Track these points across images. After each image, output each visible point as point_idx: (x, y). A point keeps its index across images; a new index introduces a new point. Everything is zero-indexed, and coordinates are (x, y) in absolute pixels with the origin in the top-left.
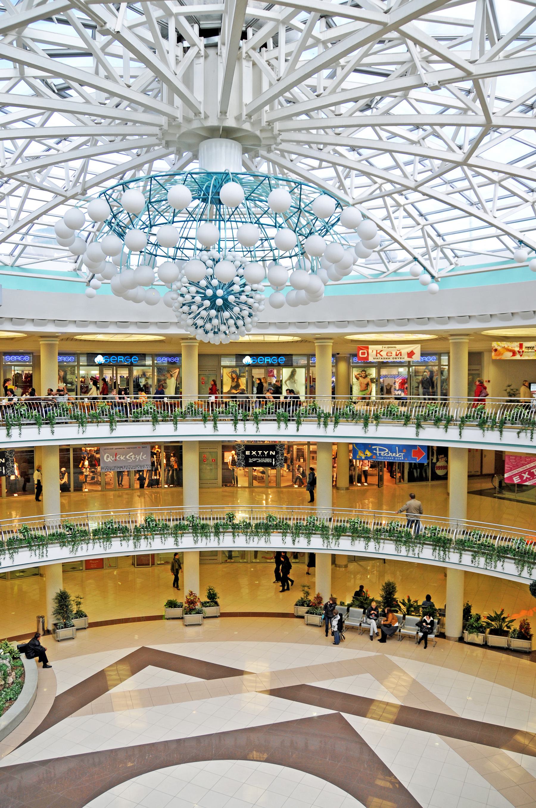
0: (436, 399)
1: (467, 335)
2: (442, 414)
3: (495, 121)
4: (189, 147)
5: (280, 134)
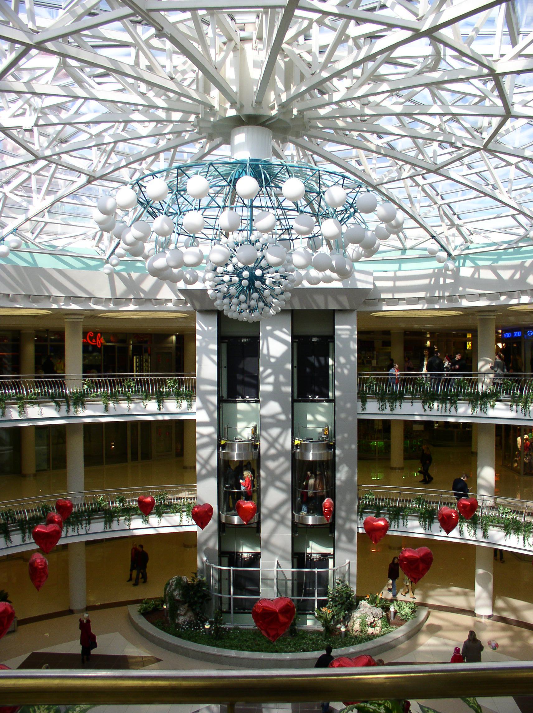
0: (132, 376)
1: (494, 311)
2: (44, 388)
3: (517, 109)
4: (220, 134)
5: (310, 122)
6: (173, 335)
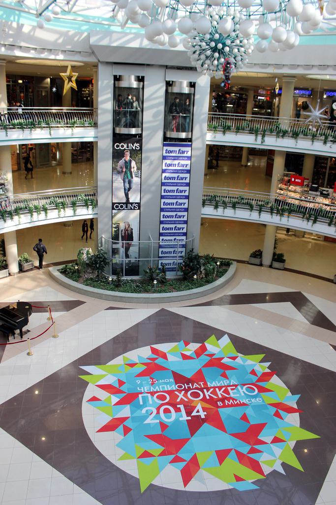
6: (45, 78)
